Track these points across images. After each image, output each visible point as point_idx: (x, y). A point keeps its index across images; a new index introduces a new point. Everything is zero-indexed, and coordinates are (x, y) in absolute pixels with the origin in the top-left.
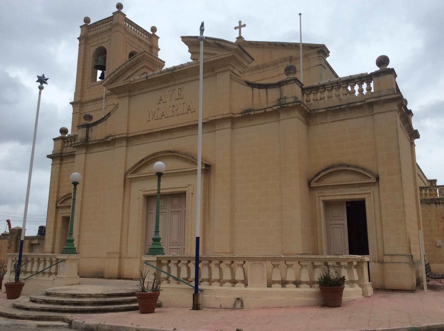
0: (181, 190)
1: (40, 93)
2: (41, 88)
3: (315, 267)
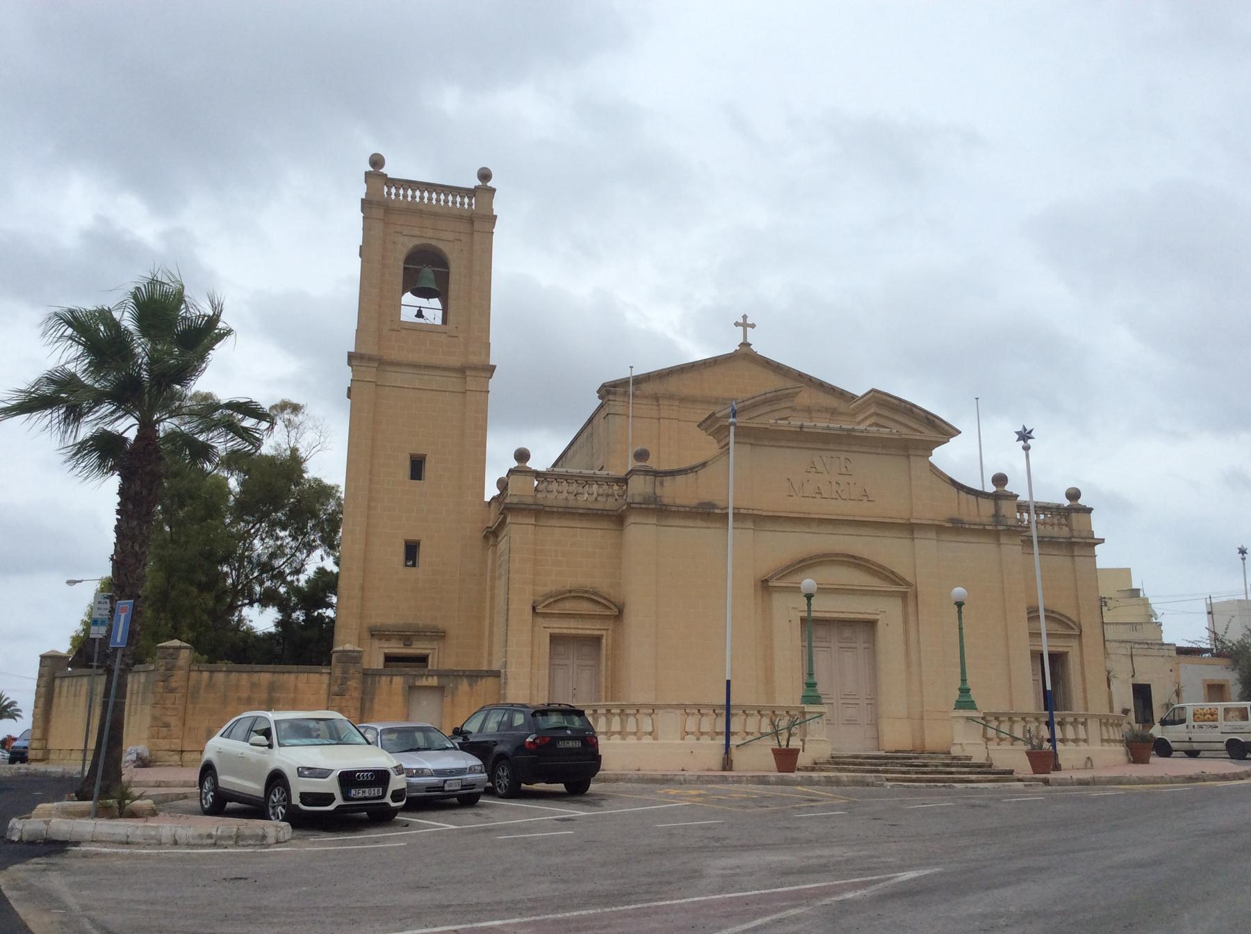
0: (869, 617)
1: (1027, 456)
2: (1027, 448)
3: (762, 716)
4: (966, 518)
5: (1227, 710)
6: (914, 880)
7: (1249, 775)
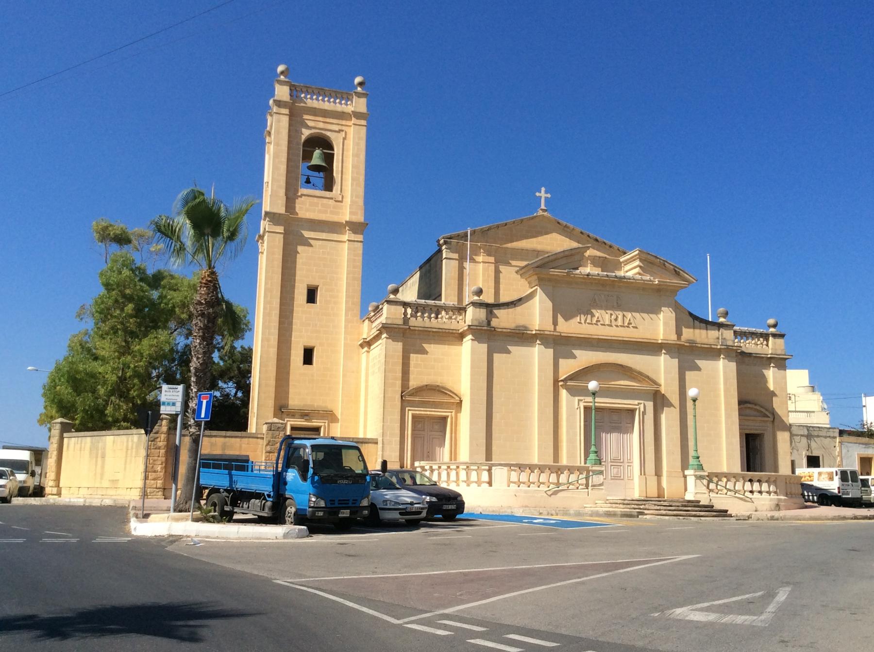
4: (698, 340)
5: (820, 474)
6: (839, 525)
7: (870, 518)
